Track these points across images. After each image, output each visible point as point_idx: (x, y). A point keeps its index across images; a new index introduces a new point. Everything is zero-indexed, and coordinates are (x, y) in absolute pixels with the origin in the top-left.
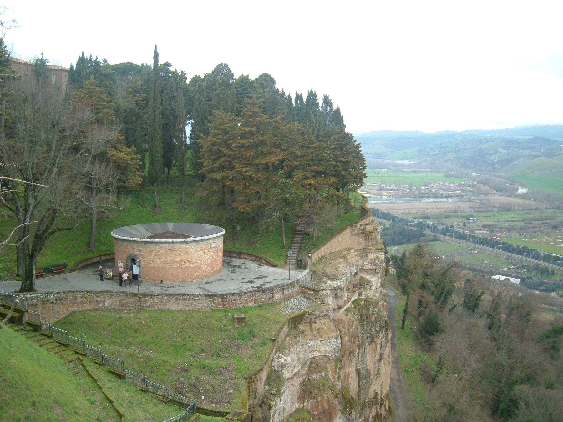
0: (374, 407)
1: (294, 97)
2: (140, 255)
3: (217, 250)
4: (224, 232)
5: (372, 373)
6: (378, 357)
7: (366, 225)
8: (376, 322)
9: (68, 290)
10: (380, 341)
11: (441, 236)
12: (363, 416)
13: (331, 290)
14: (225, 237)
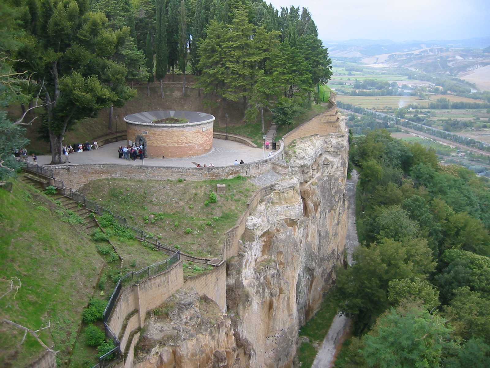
0: (331, 261)
1: (280, 11)
2: (146, 136)
3: (208, 133)
4: (214, 118)
5: (331, 234)
6: (336, 221)
7: (330, 115)
8: (336, 194)
9: (88, 165)
10: (338, 209)
11: (403, 128)
12: (322, 267)
13: (299, 167)
14: (215, 122)
